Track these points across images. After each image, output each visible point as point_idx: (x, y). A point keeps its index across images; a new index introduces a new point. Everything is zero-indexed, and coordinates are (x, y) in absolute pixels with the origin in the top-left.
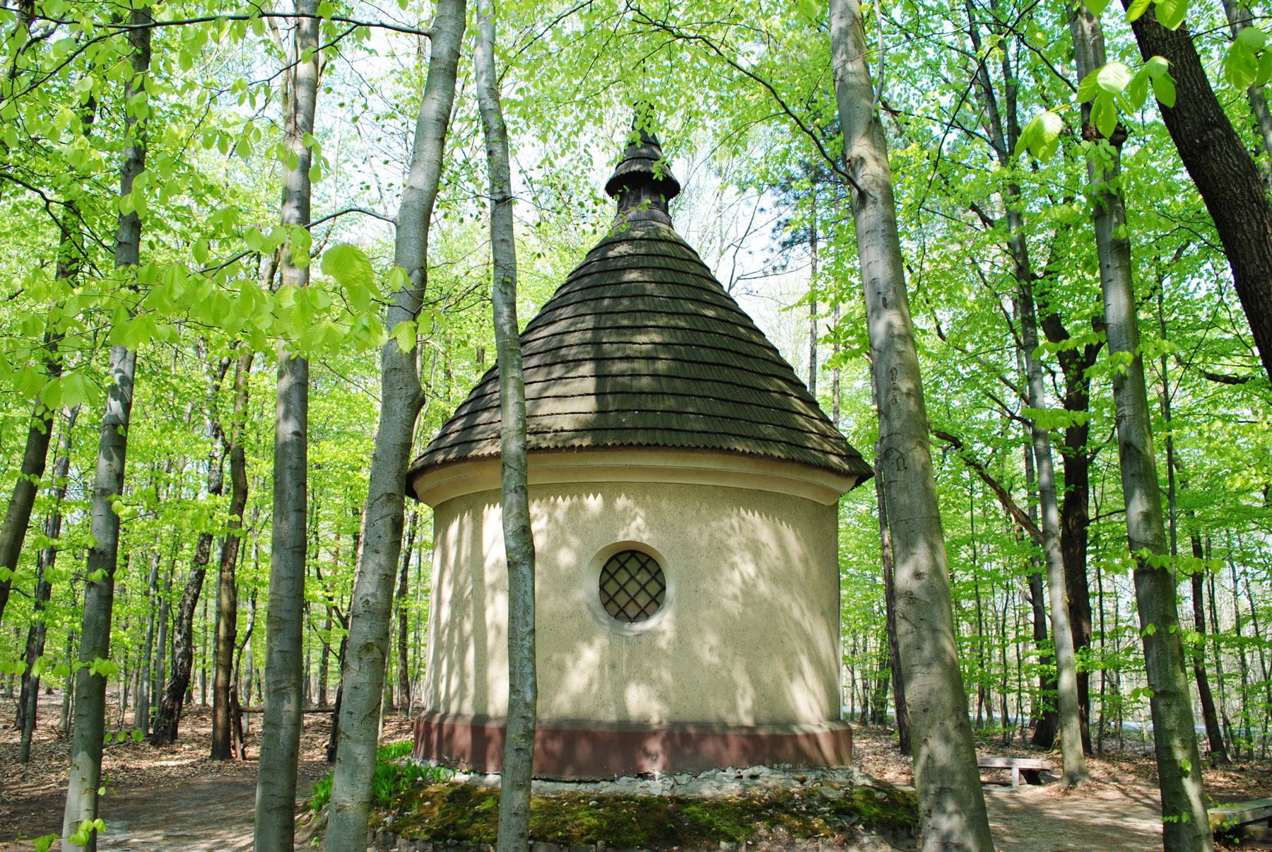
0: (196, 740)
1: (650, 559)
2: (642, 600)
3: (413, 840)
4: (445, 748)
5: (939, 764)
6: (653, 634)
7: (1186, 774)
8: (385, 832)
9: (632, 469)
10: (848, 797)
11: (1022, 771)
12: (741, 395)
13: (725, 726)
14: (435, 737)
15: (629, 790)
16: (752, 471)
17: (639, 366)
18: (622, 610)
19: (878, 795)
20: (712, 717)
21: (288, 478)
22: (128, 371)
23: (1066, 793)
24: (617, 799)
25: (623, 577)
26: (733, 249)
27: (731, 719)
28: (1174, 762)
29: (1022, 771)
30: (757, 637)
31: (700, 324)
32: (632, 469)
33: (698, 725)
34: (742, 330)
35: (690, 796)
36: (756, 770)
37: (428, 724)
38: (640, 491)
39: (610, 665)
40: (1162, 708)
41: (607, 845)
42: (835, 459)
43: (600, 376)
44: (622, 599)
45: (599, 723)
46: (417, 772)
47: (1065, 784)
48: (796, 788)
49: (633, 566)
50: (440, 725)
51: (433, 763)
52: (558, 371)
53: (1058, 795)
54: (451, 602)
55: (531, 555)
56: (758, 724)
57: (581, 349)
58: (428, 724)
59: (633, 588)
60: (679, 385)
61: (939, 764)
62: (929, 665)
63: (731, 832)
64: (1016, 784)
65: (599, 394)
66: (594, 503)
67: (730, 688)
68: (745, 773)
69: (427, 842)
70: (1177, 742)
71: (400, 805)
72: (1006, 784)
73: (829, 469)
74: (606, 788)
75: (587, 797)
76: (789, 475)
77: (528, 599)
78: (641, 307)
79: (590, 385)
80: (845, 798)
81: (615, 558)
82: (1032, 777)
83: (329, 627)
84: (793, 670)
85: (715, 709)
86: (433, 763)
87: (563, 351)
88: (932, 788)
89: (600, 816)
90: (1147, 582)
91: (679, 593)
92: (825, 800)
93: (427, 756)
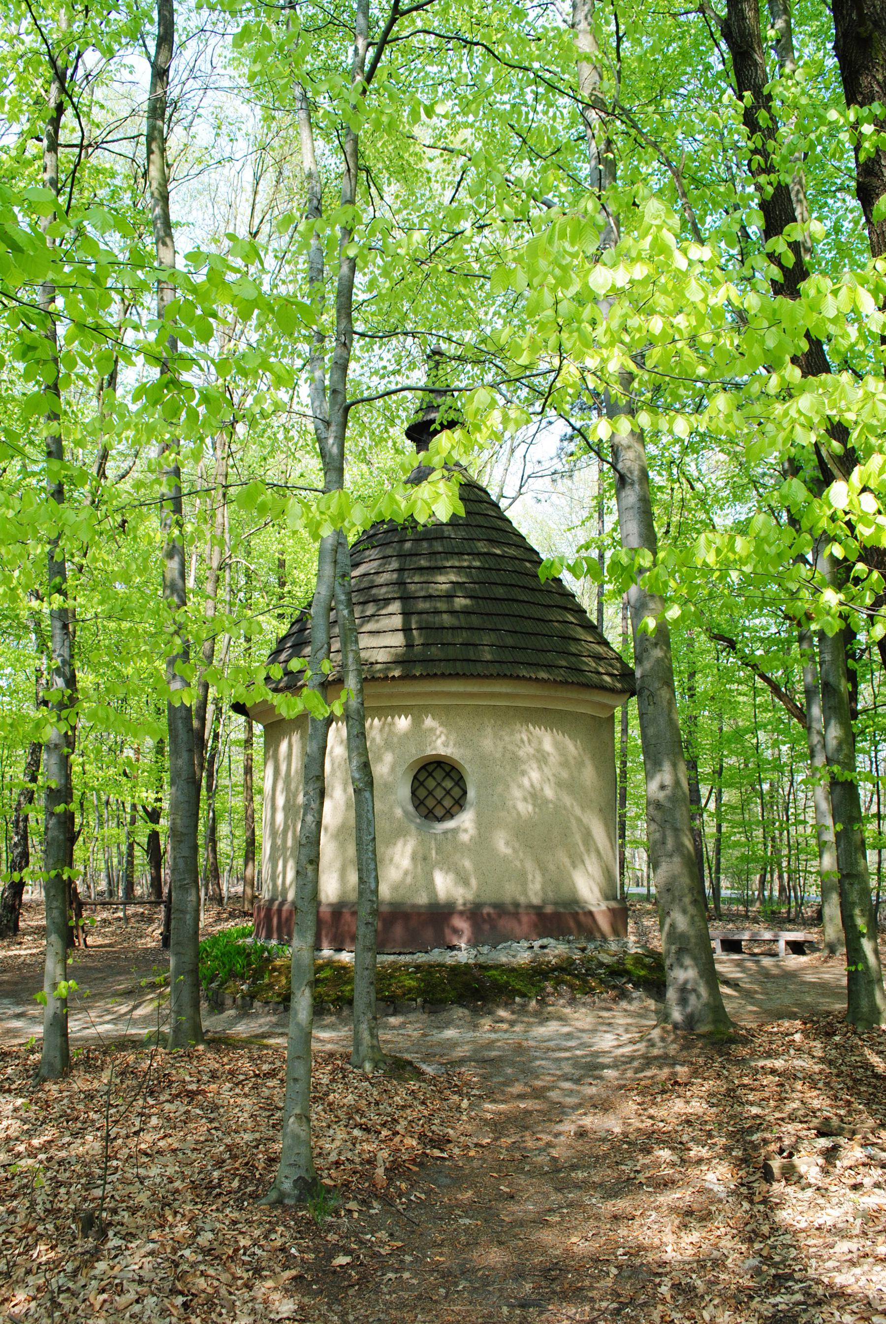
0: (40, 931)
1: (453, 768)
2: (448, 803)
3: (267, 1003)
4: (285, 930)
5: (679, 930)
6: (455, 831)
7: (863, 935)
8: (243, 997)
9: (436, 694)
10: (621, 962)
11: (788, 943)
12: (529, 626)
13: (517, 905)
14: (275, 921)
15: (440, 959)
16: (538, 693)
17: (441, 605)
18: (431, 811)
19: (647, 960)
20: (507, 898)
21: (180, 726)
22: (67, 657)
23: (825, 961)
24: (431, 966)
25: (431, 783)
26: (524, 447)
27: (522, 900)
28: (855, 926)
29: (788, 943)
30: (545, 835)
31: (491, 563)
32: (436, 694)
33: (495, 906)
34: (528, 565)
35: (490, 963)
36: (545, 941)
37: (269, 910)
38: (445, 713)
39: (421, 859)
40: (847, 886)
41: (425, 1001)
42: (607, 678)
43: (406, 614)
44: (430, 803)
45: (414, 906)
46: (264, 949)
47: (826, 953)
48: (577, 956)
49: (439, 774)
50: (279, 911)
51: (274, 942)
52: (370, 610)
53: (817, 964)
54: (284, 808)
55: (370, 783)
56: (545, 902)
57: (390, 588)
58: (269, 910)
59: (439, 793)
60: (475, 621)
61: (679, 930)
62: (671, 856)
63: (524, 990)
64: (782, 954)
65: (406, 630)
66: (403, 723)
67: (522, 878)
68: (537, 944)
69: (278, 1003)
70: (857, 911)
71: (253, 976)
72: (775, 955)
73: (603, 688)
74: (421, 958)
75: (407, 966)
76: (570, 695)
77: (370, 816)
78: (440, 549)
79: (397, 621)
80: (618, 962)
81: (424, 768)
82: (797, 948)
83: (133, 822)
84: (576, 860)
85: (510, 892)
86: (274, 942)
87: (374, 591)
88: (673, 948)
89: (418, 979)
90: (838, 789)
91: (478, 796)
92: (601, 965)
93: (269, 937)
